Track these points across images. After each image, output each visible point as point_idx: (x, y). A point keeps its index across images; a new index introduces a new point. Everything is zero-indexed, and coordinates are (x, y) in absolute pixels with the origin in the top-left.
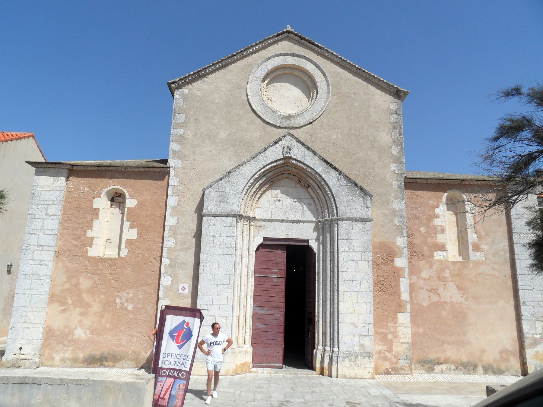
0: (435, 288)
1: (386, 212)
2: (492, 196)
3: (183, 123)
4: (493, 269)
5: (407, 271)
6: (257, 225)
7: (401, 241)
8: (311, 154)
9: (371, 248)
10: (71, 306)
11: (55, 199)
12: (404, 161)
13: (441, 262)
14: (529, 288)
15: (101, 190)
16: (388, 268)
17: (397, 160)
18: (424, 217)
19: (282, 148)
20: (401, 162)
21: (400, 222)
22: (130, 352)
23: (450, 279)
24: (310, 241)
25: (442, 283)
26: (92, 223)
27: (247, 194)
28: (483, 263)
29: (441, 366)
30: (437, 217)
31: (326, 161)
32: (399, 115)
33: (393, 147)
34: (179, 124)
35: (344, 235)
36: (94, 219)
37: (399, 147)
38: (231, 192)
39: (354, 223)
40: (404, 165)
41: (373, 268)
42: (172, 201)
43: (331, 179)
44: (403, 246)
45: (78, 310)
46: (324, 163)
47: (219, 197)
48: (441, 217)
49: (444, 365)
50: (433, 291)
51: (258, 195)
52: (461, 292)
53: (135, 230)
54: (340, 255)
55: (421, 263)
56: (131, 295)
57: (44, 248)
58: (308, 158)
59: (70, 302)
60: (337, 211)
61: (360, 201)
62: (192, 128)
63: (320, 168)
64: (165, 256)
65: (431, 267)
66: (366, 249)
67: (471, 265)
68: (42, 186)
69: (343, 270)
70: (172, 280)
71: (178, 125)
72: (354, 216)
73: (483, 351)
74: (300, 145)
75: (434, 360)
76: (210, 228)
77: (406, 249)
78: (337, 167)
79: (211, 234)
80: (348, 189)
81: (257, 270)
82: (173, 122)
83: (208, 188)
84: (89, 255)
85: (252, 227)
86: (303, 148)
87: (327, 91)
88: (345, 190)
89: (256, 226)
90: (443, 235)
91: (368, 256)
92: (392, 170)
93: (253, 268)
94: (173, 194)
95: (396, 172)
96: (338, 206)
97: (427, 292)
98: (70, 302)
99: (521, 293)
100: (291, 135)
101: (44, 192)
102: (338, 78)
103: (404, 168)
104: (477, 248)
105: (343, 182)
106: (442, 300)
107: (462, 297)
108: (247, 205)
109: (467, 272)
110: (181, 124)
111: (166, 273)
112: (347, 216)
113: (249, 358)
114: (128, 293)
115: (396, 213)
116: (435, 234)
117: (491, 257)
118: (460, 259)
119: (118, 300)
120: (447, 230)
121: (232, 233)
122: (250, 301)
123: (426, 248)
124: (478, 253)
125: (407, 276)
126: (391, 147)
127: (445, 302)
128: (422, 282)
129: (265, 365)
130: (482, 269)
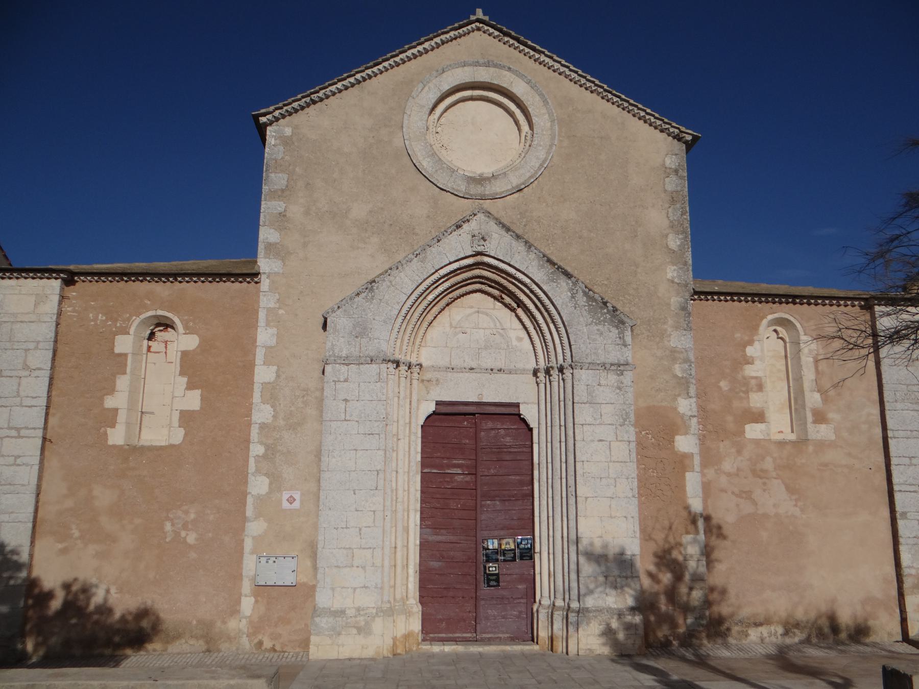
3: (283, 191)
4: (849, 454)
5: (697, 460)
6: (425, 378)
7: (686, 406)
9: (632, 417)
10: (79, 542)
11: (39, 339)
12: (690, 262)
13: (757, 442)
14: (912, 488)
15: (129, 319)
19: (470, 237)
20: (685, 263)
21: (684, 371)
22: (195, 622)
23: (774, 474)
24: (521, 407)
25: (760, 481)
26: (114, 382)
27: (406, 321)
28: (832, 445)
29: (760, 629)
30: (749, 361)
31: (549, 261)
32: (681, 178)
33: (671, 236)
34: (276, 191)
35: (585, 394)
36: (118, 373)
37: (681, 236)
38: (377, 318)
40: (691, 268)
41: (638, 454)
42: (265, 336)
43: (560, 293)
44: (690, 413)
45: (92, 548)
47: (354, 327)
48: (757, 362)
49: (764, 627)
50: (744, 495)
51: (425, 324)
52: (794, 497)
53: (197, 393)
55: (721, 445)
56: (192, 516)
57: (23, 432)
58: (517, 255)
59: (77, 534)
61: (611, 334)
63: (538, 273)
64: (256, 440)
65: (739, 452)
66: (625, 420)
67: (811, 448)
68: (13, 314)
69: (584, 458)
70: (271, 484)
71: (275, 195)
72: (602, 359)
74: (503, 232)
75: (748, 619)
76: (339, 386)
78: (569, 270)
79: (342, 397)
80: (590, 311)
81: (426, 461)
82: (265, 188)
83: (333, 311)
84: (110, 443)
85: (415, 382)
86: (508, 238)
88: (585, 313)
89: (423, 381)
90: (760, 394)
91: (627, 432)
92: (669, 276)
93: (419, 458)
94: (268, 324)
95: (676, 280)
96: (572, 343)
98: (77, 534)
99: (898, 497)
100: (488, 214)
101: (18, 325)
102: (570, 109)
104: (820, 417)
105: (582, 300)
106: (760, 512)
107: (796, 505)
108: (406, 341)
109: (804, 461)
110: (280, 193)
111: (258, 471)
113: (416, 625)
114: (186, 512)
115: (677, 355)
116: (747, 392)
119: (168, 527)
120: (768, 386)
121: (379, 394)
122: (415, 519)
123: (730, 418)
124: (823, 427)
125: (697, 468)
126: (667, 236)
127: (766, 516)
128: (723, 480)
129: (444, 635)
130: (830, 456)
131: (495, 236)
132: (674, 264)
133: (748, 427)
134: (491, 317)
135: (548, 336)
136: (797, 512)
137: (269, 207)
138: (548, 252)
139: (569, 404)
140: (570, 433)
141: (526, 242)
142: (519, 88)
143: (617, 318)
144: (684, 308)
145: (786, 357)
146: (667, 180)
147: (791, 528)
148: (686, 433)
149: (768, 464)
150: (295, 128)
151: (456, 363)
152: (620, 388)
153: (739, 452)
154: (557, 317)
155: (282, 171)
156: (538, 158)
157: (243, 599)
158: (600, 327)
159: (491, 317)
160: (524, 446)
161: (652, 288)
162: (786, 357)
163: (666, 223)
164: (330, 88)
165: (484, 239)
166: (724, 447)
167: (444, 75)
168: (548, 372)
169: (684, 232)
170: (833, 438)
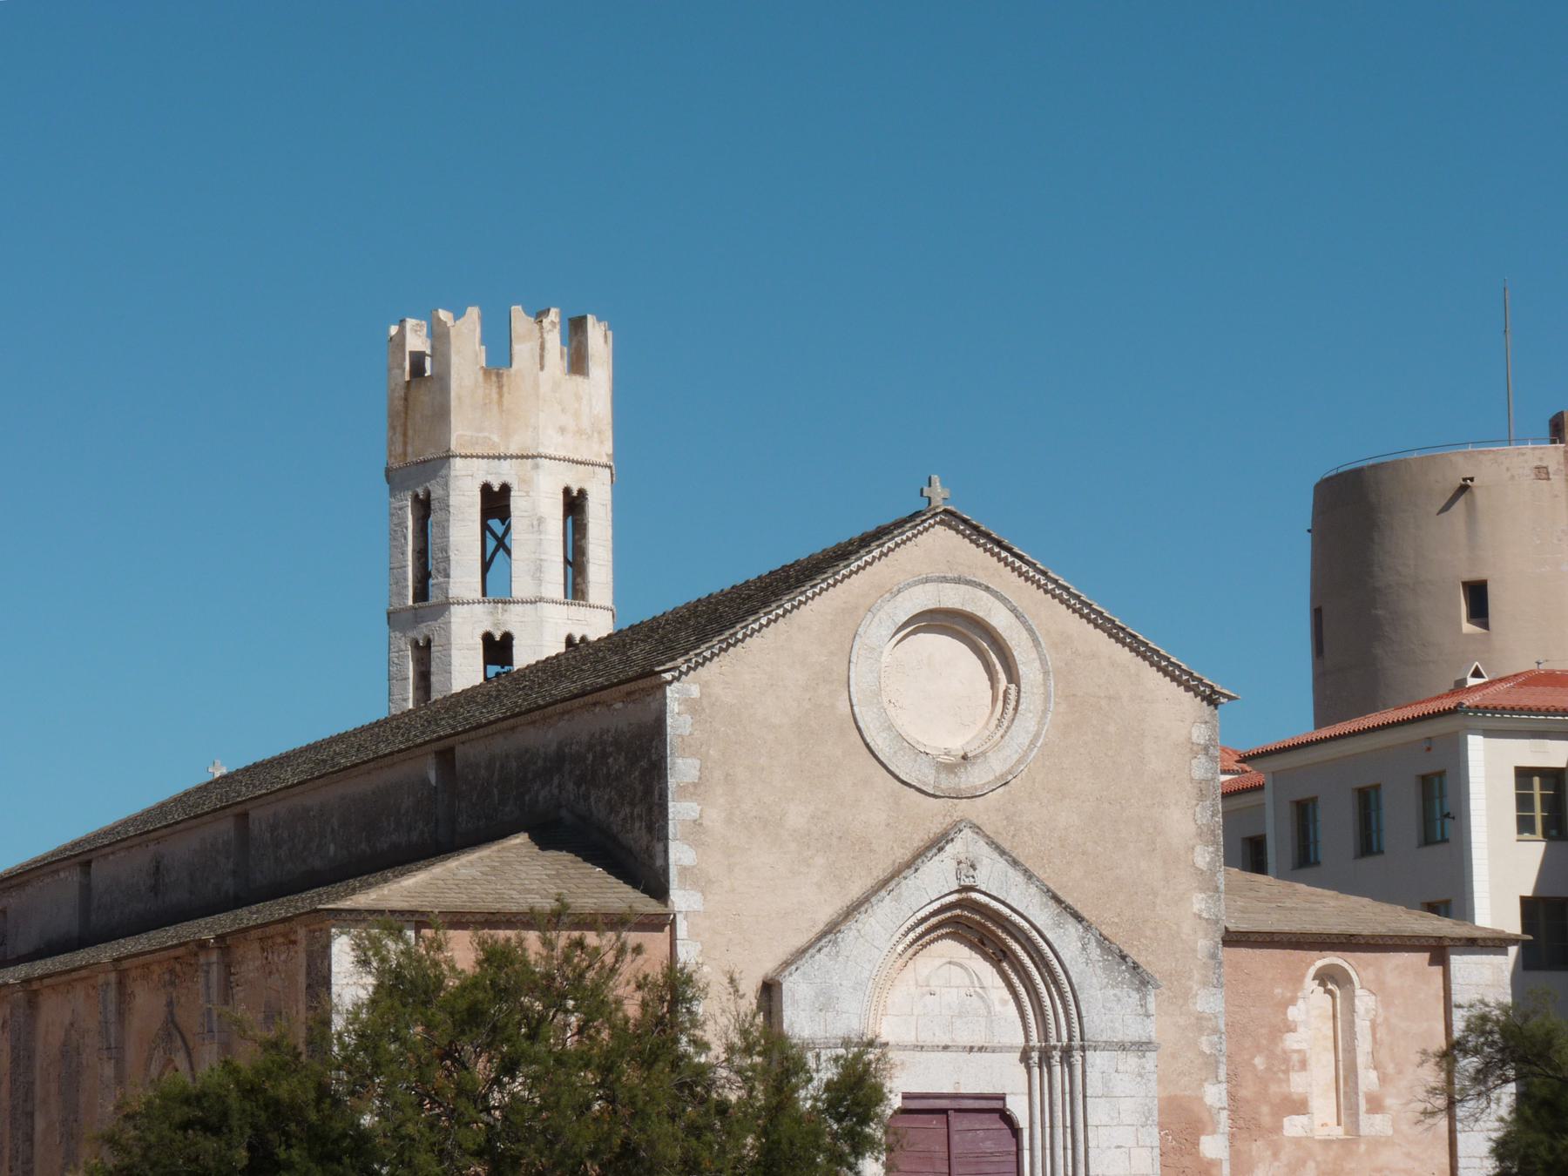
1: (1182, 1021)
3: (695, 785)
4: (1408, 1155)
7: (1215, 1095)
8: (1019, 878)
12: (1222, 887)
13: (1297, 1141)
16: (1187, 1161)
17: (1207, 883)
18: (1263, 1031)
20: (1216, 889)
21: (1212, 1045)
28: (1386, 1142)
30: (1291, 1028)
31: (1057, 899)
33: (1198, 849)
39: (1121, 1055)
43: (1067, 943)
44: (1219, 1105)
46: (1051, 903)
47: (817, 996)
48: (1301, 1029)
54: (1090, 1135)
55: (1254, 1146)
60: (1081, 1024)
62: (721, 801)
65: (1275, 1155)
67: (1363, 1148)
71: (684, 791)
72: (1119, 1037)
73: (1501, 1119)
74: (996, 855)
77: (1224, 1114)
80: (1104, 969)
86: (1002, 863)
87: (1042, 690)
88: (1099, 972)
92: (1196, 908)
95: (1205, 915)
96: (1084, 1014)
100: (977, 829)
103: (1223, 907)
104: (1376, 1106)
105: (1095, 952)
109: (1353, 1165)
110: (691, 789)
112: (1104, 1038)
116: (1286, 1072)
117: (1405, 1127)
118: (1338, 1132)
120: (1312, 1062)
123: (1265, 1109)
124: (1379, 1117)
131: (986, 861)
132: (1202, 890)
133: (1286, 1121)
134: (966, 969)
135: (1047, 1002)
137: (680, 811)
138: (1052, 887)
139: (1076, 1097)
140: (1081, 1137)
141: (1026, 871)
142: (1000, 619)
143: (1141, 978)
144: (1213, 956)
145: (1334, 1016)
146: (1194, 762)
148: (1214, 1132)
150: (704, 685)
151: (926, 1038)
152: (1141, 1075)
153: (1275, 1155)
154: (1063, 977)
155: (693, 755)
156: (1027, 732)
158: (1117, 991)
159: (966, 969)
160: (1009, 1153)
162: (1334, 1016)
163: (1192, 828)
165: (973, 866)
166: (1258, 1148)
167: (899, 598)
168: (1045, 1058)
169: (1214, 843)
170: (1390, 1132)
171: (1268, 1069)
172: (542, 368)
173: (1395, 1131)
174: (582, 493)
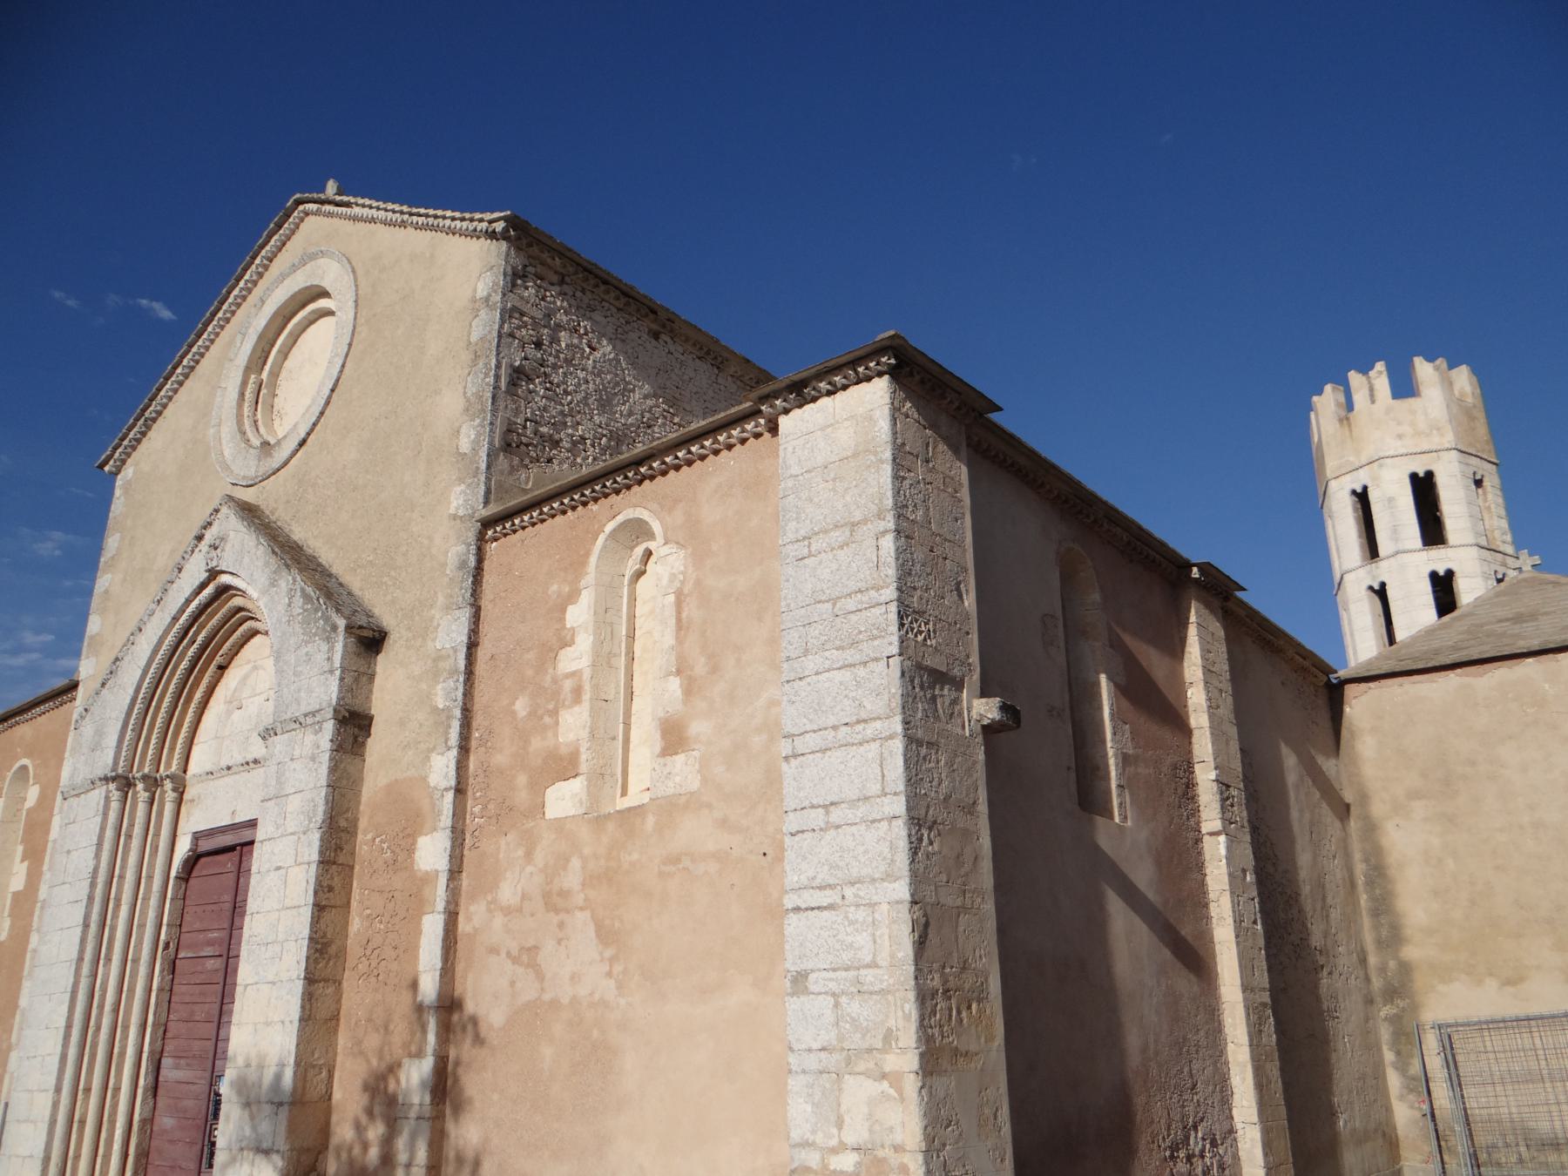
0: (531, 942)
2: (994, 417)
4: (723, 823)
23: (579, 899)
52: (608, 953)
55: (503, 842)
65: (529, 855)
92: (452, 511)
97: (509, 965)
107: (609, 974)
109: (635, 856)
116: (554, 713)
124: (680, 759)
127: (554, 1004)
132: (461, 480)
136: (608, 988)
147: (595, 1033)
149: (572, 878)
157: (1208, 842)
161: (426, 542)
164: (162, 393)
171: (533, 714)
172: (1373, 402)
173: (704, 781)
174: (1430, 475)
